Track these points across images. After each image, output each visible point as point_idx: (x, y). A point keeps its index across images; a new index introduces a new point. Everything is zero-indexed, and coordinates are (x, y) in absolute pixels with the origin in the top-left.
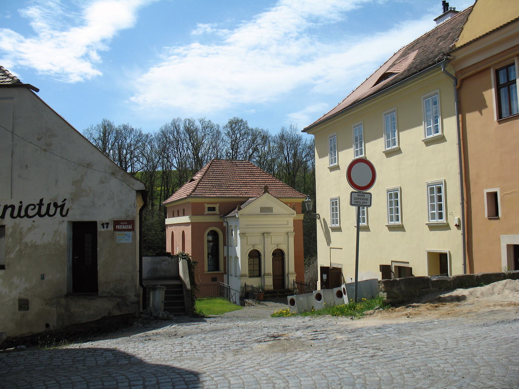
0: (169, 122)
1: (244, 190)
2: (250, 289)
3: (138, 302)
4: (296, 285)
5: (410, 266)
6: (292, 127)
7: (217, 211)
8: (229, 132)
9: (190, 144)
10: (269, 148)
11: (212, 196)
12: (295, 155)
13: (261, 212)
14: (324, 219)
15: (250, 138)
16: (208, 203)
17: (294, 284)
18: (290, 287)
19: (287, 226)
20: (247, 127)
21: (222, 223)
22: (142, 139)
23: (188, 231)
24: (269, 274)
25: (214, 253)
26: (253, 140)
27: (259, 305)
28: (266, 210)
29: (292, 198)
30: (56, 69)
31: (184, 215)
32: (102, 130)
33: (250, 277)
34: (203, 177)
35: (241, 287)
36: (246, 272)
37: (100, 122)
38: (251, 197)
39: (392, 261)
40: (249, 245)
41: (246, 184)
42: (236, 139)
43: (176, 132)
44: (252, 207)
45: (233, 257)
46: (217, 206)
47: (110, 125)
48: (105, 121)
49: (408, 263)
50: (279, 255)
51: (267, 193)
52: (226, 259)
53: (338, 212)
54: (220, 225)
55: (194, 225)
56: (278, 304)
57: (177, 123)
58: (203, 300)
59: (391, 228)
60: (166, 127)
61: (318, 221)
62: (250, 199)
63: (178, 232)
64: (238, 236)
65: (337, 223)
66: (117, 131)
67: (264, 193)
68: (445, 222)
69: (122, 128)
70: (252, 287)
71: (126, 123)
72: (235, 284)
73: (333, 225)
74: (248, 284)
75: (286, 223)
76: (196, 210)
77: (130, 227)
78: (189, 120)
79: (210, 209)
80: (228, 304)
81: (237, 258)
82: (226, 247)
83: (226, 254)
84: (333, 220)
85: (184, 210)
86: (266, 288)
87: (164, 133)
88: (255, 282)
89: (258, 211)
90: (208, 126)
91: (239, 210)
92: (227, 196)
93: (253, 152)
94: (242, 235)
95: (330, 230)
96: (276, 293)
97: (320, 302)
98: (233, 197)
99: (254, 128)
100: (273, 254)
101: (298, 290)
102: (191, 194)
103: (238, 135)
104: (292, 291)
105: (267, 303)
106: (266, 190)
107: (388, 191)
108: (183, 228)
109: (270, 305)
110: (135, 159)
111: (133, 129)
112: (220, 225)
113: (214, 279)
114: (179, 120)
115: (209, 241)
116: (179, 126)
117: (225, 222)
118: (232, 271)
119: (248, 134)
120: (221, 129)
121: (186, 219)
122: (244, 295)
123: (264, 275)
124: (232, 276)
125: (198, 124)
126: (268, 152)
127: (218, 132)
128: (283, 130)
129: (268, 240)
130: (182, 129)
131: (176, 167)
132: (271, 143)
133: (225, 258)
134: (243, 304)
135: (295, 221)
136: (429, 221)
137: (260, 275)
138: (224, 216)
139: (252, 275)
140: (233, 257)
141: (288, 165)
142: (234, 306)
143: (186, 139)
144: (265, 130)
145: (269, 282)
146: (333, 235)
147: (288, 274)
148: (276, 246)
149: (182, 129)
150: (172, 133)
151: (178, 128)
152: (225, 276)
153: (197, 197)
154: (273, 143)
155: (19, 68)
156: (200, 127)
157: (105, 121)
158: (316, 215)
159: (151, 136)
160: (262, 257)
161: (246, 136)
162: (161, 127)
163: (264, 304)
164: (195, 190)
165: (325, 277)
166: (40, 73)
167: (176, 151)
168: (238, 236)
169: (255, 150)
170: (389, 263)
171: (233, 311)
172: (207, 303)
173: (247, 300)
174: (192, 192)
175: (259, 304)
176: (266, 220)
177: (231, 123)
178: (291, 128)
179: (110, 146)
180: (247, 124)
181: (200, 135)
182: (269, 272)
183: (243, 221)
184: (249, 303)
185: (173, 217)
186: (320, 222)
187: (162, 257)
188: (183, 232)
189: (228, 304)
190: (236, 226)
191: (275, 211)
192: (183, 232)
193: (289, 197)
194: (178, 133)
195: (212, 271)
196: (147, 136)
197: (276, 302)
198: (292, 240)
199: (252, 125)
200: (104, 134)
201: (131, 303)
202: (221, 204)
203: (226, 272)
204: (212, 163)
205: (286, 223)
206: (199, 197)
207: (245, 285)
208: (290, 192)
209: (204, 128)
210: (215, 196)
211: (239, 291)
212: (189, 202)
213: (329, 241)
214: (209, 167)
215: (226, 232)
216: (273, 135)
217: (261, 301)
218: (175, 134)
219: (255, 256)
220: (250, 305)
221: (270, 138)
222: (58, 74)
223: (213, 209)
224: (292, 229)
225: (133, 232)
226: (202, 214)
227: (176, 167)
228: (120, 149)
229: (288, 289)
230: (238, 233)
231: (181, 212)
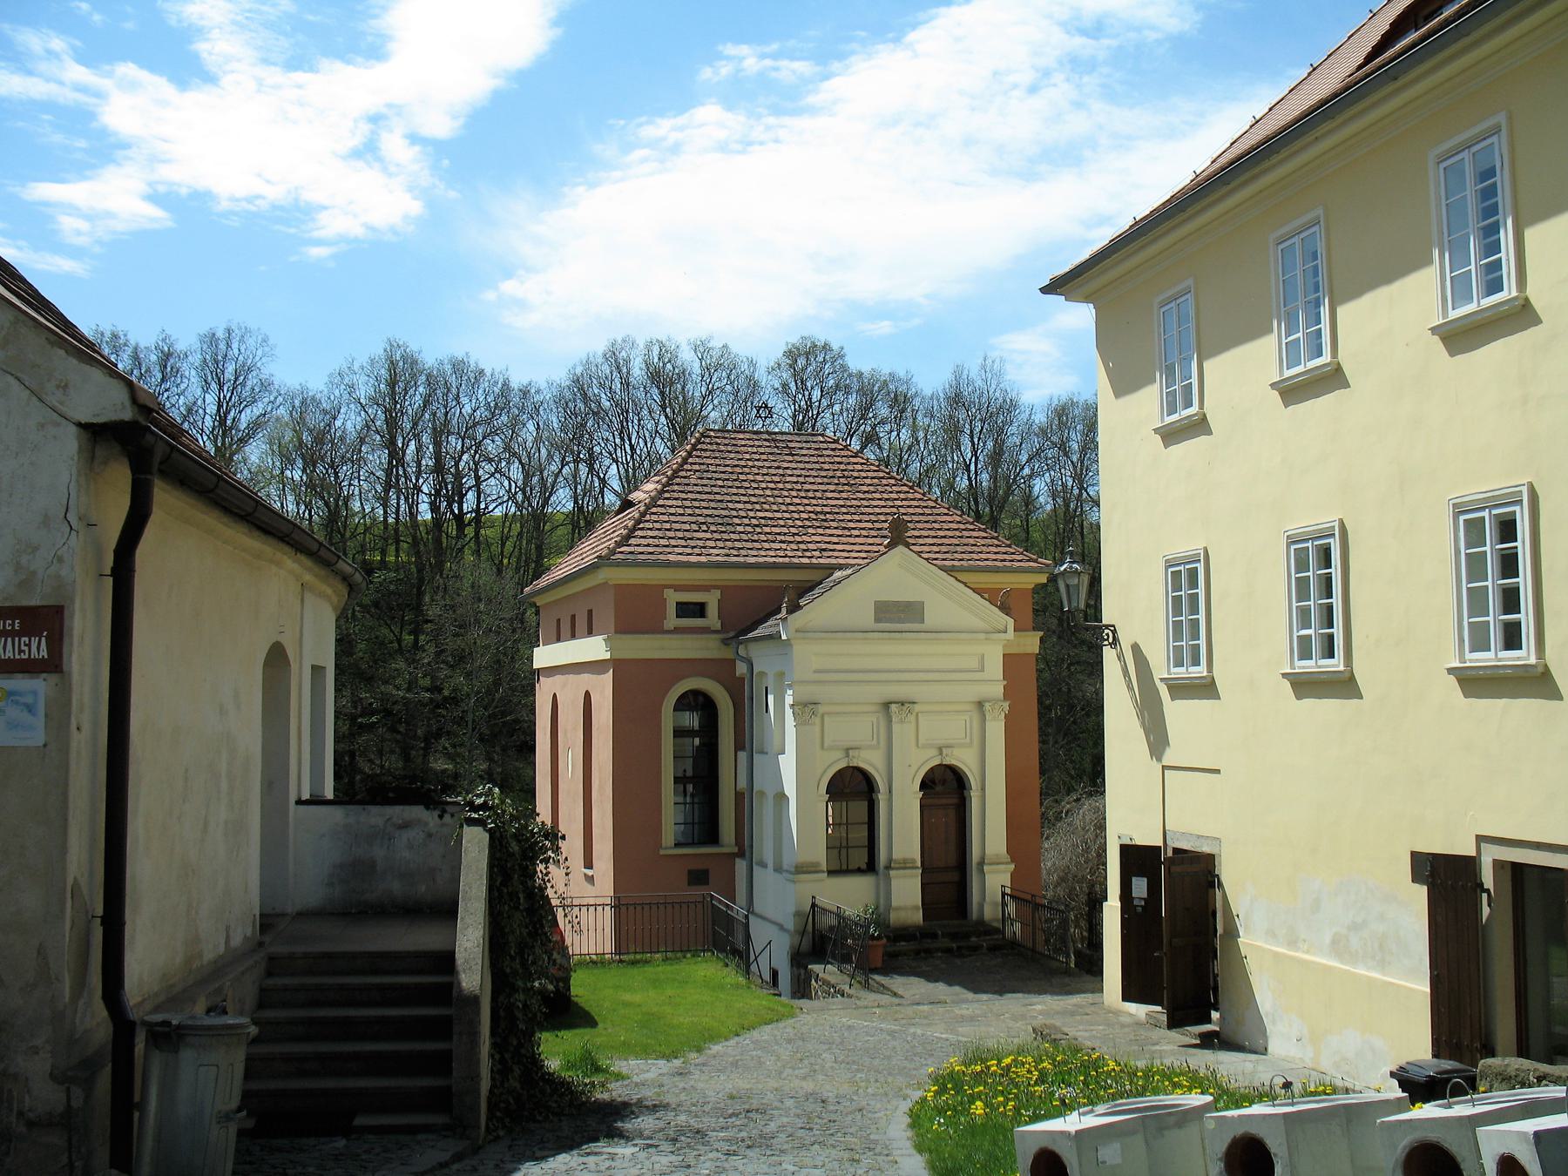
0: (599, 347)
1: (815, 538)
3: (66, 1121)
4: (1011, 908)
7: (713, 618)
8: (785, 386)
9: (663, 419)
11: (693, 559)
12: (996, 457)
13: (877, 620)
14: (1136, 648)
16: (678, 588)
17: (1004, 904)
18: (990, 913)
19: (978, 676)
20: (844, 368)
22: (509, 404)
23: (603, 688)
24: (905, 865)
25: (702, 779)
26: (865, 408)
27: (864, 994)
28: (898, 615)
29: (997, 570)
31: (590, 633)
33: (831, 873)
34: (662, 492)
35: (797, 914)
36: (819, 854)
37: (378, 350)
38: (841, 567)
39: (1480, 839)
40: (831, 748)
41: (822, 519)
42: (810, 405)
43: (617, 381)
44: (845, 602)
45: (770, 795)
46: (712, 600)
47: (412, 362)
48: (392, 346)
50: (946, 789)
51: (901, 548)
52: (743, 800)
53: (1202, 616)
54: (723, 670)
55: (620, 668)
56: (941, 989)
58: (647, 962)
61: (1109, 654)
62: (838, 574)
63: (569, 691)
64: (789, 712)
66: (429, 376)
67: (890, 546)
71: (460, 355)
72: (775, 904)
73: (1180, 672)
74: (823, 901)
75: (974, 664)
76: (634, 613)
77: (38, 648)
78: (662, 345)
79: (684, 610)
80: (737, 986)
81: (782, 797)
82: (742, 755)
83: (742, 784)
84: (1178, 651)
85: (590, 612)
86: (895, 918)
87: (579, 386)
88: (849, 897)
89: (867, 618)
90: (718, 365)
91: (791, 611)
92: (752, 560)
93: (863, 447)
94: (805, 708)
95: (1163, 690)
96: (934, 936)
98: (775, 566)
99: (866, 368)
100: (923, 786)
101: (1017, 927)
103: (816, 394)
104: (997, 931)
105: (897, 982)
106: (898, 535)
107: (1459, 510)
109: (907, 994)
111: (482, 372)
112: (723, 670)
113: (698, 877)
114: (629, 342)
115: (679, 733)
116: (627, 361)
117: (743, 659)
118: (765, 846)
120: (762, 376)
121: (593, 648)
122: (806, 944)
123: (888, 867)
124: (764, 865)
125: (687, 357)
126: (910, 448)
127: (754, 386)
128: (958, 375)
129: (903, 731)
130: (638, 372)
131: (615, 492)
133: (739, 796)
134: (802, 989)
135: (1011, 662)
137: (871, 867)
138: (737, 636)
140: (770, 795)
141: (973, 489)
142: (760, 999)
143: (661, 411)
144: (902, 374)
145: (906, 896)
146: (1176, 712)
147: (981, 863)
149: (638, 372)
151: (624, 370)
152: (741, 866)
156: (697, 370)
157: (392, 346)
158: (1101, 628)
159: (538, 392)
160: (882, 798)
161: (840, 396)
163: (884, 989)
164: (628, 537)
165: (1140, 887)
167: (618, 441)
168: (789, 712)
169: (870, 439)
172: (656, 983)
173: (816, 968)
174: (618, 544)
175: (866, 986)
176: (900, 654)
177: (792, 355)
178: (984, 367)
180: (842, 357)
181: (696, 390)
182: (908, 856)
185: (558, 640)
186: (1120, 657)
187: (398, 809)
188: (587, 695)
189: (737, 986)
191: (931, 619)
192: (587, 695)
194: (626, 384)
195: (692, 844)
196: (525, 393)
197: (931, 977)
199: (859, 362)
200: (392, 384)
201: (31, 1124)
202: (725, 590)
203: (744, 849)
204: (698, 441)
205: (974, 664)
206: (644, 564)
207: (814, 905)
208: (988, 548)
209: (708, 370)
210: (703, 559)
213: (1157, 739)
214: (690, 455)
215: (744, 695)
216: (928, 392)
218: (617, 386)
219: (853, 789)
220: (833, 991)
221: (917, 402)
223: (699, 610)
224: (998, 690)
225: (53, 678)
226: (654, 627)
227: (615, 492)
228: (438, 436)
229: (981, 922)
230: (789, 700)
231: (581, 623)
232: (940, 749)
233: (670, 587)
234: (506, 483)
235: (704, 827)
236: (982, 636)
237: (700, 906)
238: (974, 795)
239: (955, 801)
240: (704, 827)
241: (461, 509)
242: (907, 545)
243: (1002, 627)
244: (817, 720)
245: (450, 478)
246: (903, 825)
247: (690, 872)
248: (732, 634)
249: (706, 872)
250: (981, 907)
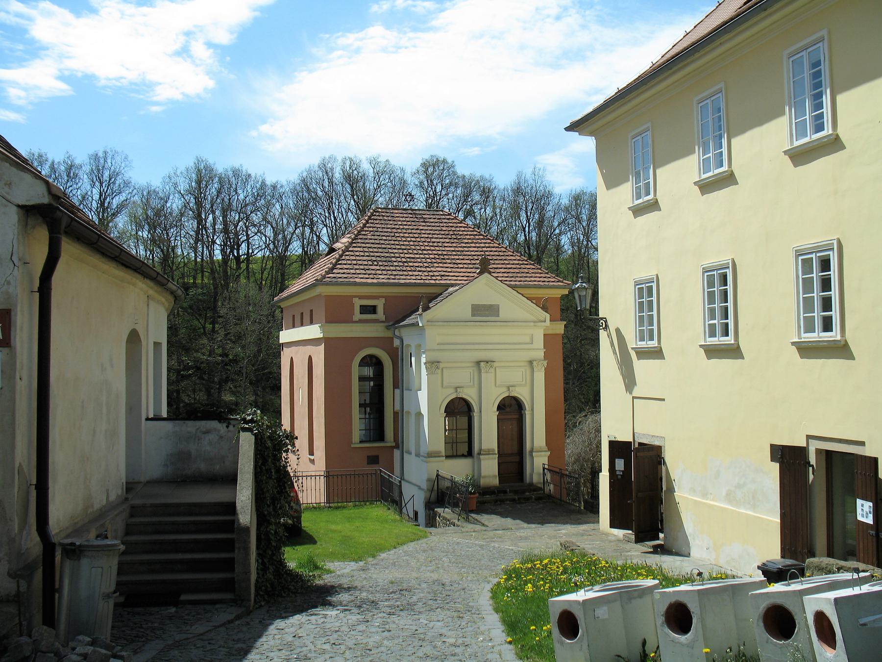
0: (315, 161)
1: (438, 269)
2: (448, 484)
4: (548, 476)
5: (868, 451)
6: (537, 170)
7: (380, 314)
8: (421, 183)
9: (352, 202)
10: (494, 208)
11: (369, 281)
12: (540, 223)
13: (473, 315)
14: (618, 331)
15: (459, 191)
16: (361, 297)
17: (544, 474)
18: (537, 479)
20: (454, 173)
21: (391, 340)
22: (265, 194)
23: (319, 354)
24: (489, 452)
25: (375, 405)
26: (467, 196)
28: (484, 312)
29: (540, 287)
30: (132, 76)
31: (311, 323)
32: (194, 176)
33: (447, 457)
34: (352, 243)
35: (429, 480)
36: (441, 447)
37: (190, 163)
38: (452, 285)
39: (809, 437)
40: (447, 387)
41: (442, 258)
43: (326, 181)
46: (380, 304)
47: (209, 169)
48: (199, 160)
49: (862, 444)
50: (511, 410)
51: (486, 274)
52: (398, 417)
54: (386, 343)
55: (330, 344)
56: (509, 521)
57: (330, 165)
58: (344, 507)
59: (712, 352)
60: (309, 171)
61: (603, 334)
62: (451, 289)
63: (300, 356)
64: (423, 367)
65: (652, 339)
66: (220, 178)
67: (480, 273)
68: (839, 338)
69: (230, 174)
70: (452, 480)
72: (416, 475)
73: (643, 344)
74: (442, 473)
75: (528, 340)
76: (336, 311)
78: (351, 160)
79: (365, 309)
80: (394, 521)
81: (419, 415)
82: (397, 391)
83: (398, 407)
85: (311, 311)
86: (483, 482)
88: (457, 471)
89: (468, 314)
90: (383, 171)
91: (424, 310)
92: (403, 281)
94: (433, 365)
95: (633, 354)
96: (505, 492)
97: (683, 638)
98: (415, 285)
100: (499, 408)
102: (324, 277)
103: (439, 188)
104: (540, 489)
105: (485, 518)
106: (485, 267)
108: (310, 350)
109: (490, 525)
110: (254, 230)
111: (249, 175)
112: (386, 343)
113: (373, 460)
114: (332, 158)
115: (362, 379)
116: (332, 169)
118: (410, 442)
119: (457, 186)
120: (408, 177)
121: (313, 331)
122: (434, 497)
123: (479, 454)
124: (410, 453)
125: (366, 167)
127: (403, 183)
128: (519, 176)
130: (338, 175)
131: (325, 243)
132: (497, 201)
133: (396, 414)
134: (431, 522)
136: (705, 341)
137: (470, 454)
138: (394, 324)
139: (450, 453)
142: (408, 528)
143: (351, 199)
144: (487, 177)
145: (489, 470)
146: (641, 367)
147: (531, 451)
148: (505, 389)
149: (338, 175)
150: (320, 183)
152: (397, 453)
153: (337, 284)
154: (501, 203)
155: (67, 73)
159: (282, 187)
160: (476, 415)
161: (452, 189)
162: (300, 172)
164: (333, 268)
165: (620, 464)
166: (103, 82)
168: (423, 367)
169: (469, 213)
170: (800, 442)
171: (403, 544)
172: (349, 519)
173: (439, 510)
174: (327, 273)
175: (467, 520)
177: (425, 165)
179: (208, 206)
181: (370, 186)
182: (491, 447)
183: (434, 336)
184: (444, 518)
185: (294, 327)
186: (609, 336)
188: (310, 358)
189: (394, 521)
190: (419, 346)
191: (503, 314)
192: (310, 358)
193: (535, 287)
194: (331, 182)
195: (369, 441)
196: (274, 187)
198: (540, 377)
199: (463, 170)
200: (199, 182)
203: (398, 444)
204: (372, 214)
205: (528, 340)
206: (342, 284)
207: (438, 475)
208: (535, 275)
209: (378, 174)
210: (375, 281)
211: (424, 486)
212: (319, 296)
213: (630, 381)
214: (367, 222)
215: (398, 357)
216: (502, 187)
217: (472, 511)
218: (326, 184)
219: (459, 410)
220: (449, 523)
221: (495, 192)
222: (135, 84)
223: (373, 310)
224: (541, 354)
227: (325, 243)
229: (531, 484)
230: (423, 360)
231: (307, 318)
232: (508, 388)
233: (356, 297)
234: (264, 238)
235: (376, 431)
236: (532, 324)
237: (374, 476)
238: (528, 414)
239: (516, 416)
240: (376, 431)
241: (238, 253)
242: (490, 273)
243: (542, 319)
244: (439, 371)
245: (232, 236)
246: (488, 431)
248: (391, 323)
249: (377, 457)
250: (531, 476)
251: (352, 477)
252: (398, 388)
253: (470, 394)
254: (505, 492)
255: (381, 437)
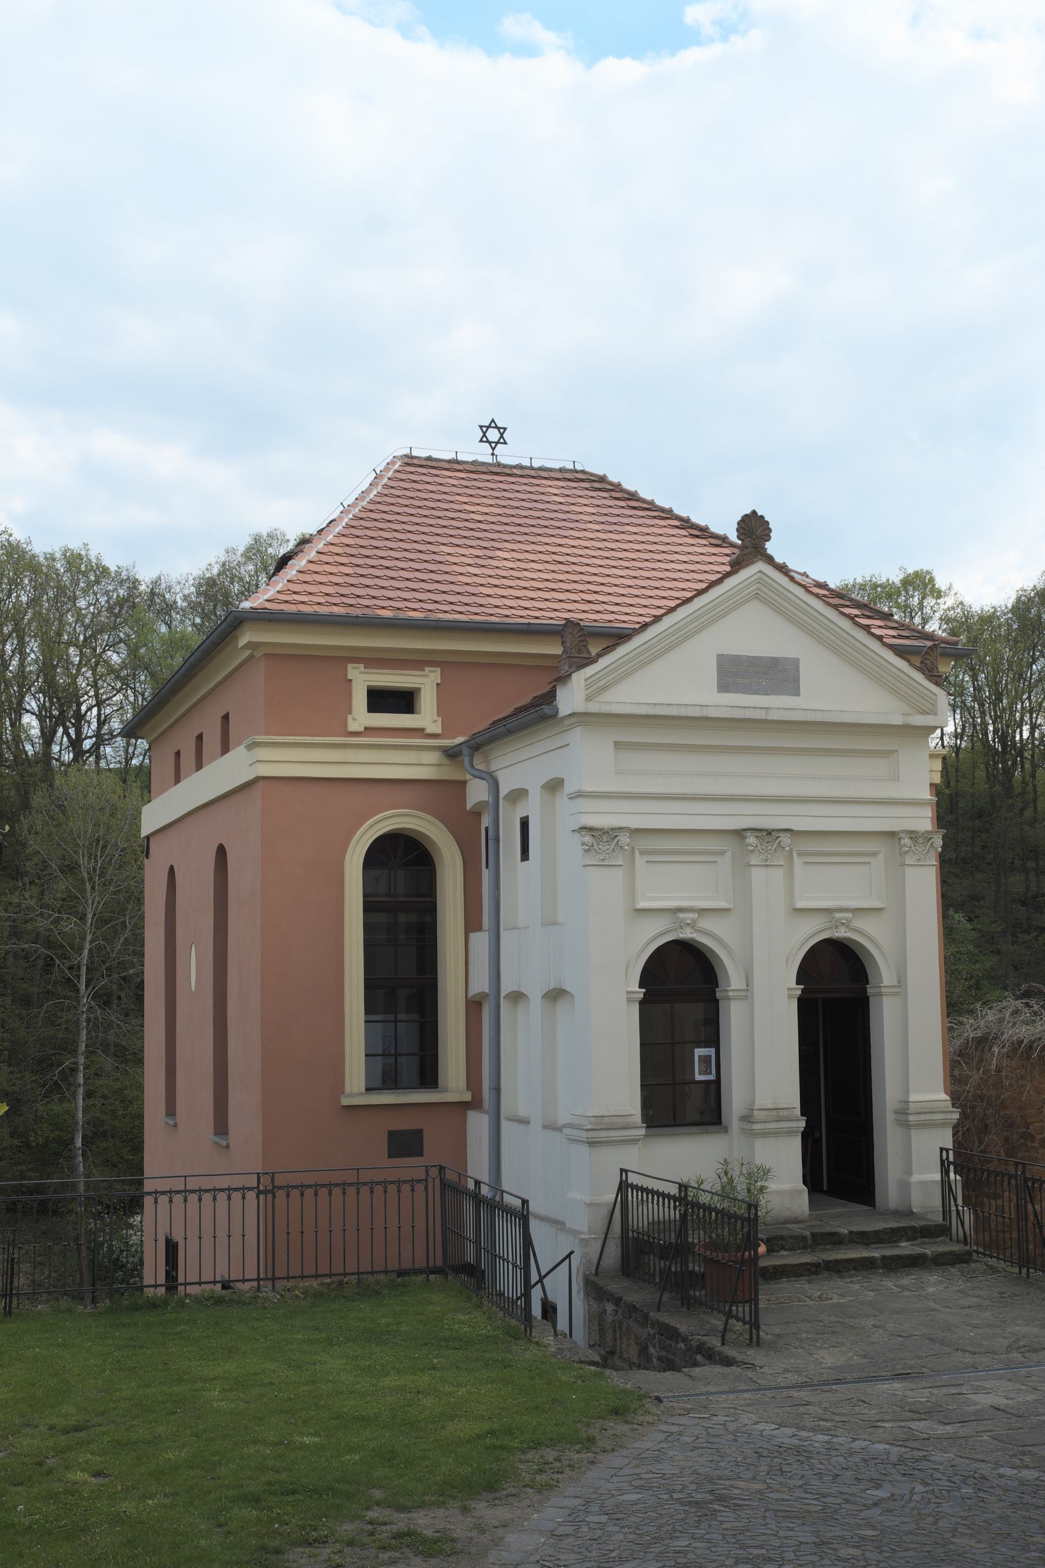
0: (242, 543)
45: (535, 993)
50: (836, 992)
54: (444, 796)
71: (75, 545)
79: (382, 700)
82: (481, 940)
117: (480, 775)
133: (474, 1005)
140: (535, 993)
152: (478, 1123)
198: (923, 884)
207: (624, 1187)
219: (681, 985)
223: (403, 701)
237: (420, 1188)
241: (79, 732)
246: (763, 1052)
247: (392, 1134)
249: (419, 1133)
250: (905, 1186)
251: (351, 1191)
252: (479, 928)
253: (716, 936)
254: (835, 1240)
255: (428, 1075)
